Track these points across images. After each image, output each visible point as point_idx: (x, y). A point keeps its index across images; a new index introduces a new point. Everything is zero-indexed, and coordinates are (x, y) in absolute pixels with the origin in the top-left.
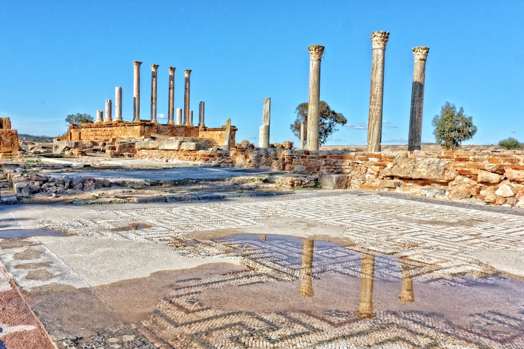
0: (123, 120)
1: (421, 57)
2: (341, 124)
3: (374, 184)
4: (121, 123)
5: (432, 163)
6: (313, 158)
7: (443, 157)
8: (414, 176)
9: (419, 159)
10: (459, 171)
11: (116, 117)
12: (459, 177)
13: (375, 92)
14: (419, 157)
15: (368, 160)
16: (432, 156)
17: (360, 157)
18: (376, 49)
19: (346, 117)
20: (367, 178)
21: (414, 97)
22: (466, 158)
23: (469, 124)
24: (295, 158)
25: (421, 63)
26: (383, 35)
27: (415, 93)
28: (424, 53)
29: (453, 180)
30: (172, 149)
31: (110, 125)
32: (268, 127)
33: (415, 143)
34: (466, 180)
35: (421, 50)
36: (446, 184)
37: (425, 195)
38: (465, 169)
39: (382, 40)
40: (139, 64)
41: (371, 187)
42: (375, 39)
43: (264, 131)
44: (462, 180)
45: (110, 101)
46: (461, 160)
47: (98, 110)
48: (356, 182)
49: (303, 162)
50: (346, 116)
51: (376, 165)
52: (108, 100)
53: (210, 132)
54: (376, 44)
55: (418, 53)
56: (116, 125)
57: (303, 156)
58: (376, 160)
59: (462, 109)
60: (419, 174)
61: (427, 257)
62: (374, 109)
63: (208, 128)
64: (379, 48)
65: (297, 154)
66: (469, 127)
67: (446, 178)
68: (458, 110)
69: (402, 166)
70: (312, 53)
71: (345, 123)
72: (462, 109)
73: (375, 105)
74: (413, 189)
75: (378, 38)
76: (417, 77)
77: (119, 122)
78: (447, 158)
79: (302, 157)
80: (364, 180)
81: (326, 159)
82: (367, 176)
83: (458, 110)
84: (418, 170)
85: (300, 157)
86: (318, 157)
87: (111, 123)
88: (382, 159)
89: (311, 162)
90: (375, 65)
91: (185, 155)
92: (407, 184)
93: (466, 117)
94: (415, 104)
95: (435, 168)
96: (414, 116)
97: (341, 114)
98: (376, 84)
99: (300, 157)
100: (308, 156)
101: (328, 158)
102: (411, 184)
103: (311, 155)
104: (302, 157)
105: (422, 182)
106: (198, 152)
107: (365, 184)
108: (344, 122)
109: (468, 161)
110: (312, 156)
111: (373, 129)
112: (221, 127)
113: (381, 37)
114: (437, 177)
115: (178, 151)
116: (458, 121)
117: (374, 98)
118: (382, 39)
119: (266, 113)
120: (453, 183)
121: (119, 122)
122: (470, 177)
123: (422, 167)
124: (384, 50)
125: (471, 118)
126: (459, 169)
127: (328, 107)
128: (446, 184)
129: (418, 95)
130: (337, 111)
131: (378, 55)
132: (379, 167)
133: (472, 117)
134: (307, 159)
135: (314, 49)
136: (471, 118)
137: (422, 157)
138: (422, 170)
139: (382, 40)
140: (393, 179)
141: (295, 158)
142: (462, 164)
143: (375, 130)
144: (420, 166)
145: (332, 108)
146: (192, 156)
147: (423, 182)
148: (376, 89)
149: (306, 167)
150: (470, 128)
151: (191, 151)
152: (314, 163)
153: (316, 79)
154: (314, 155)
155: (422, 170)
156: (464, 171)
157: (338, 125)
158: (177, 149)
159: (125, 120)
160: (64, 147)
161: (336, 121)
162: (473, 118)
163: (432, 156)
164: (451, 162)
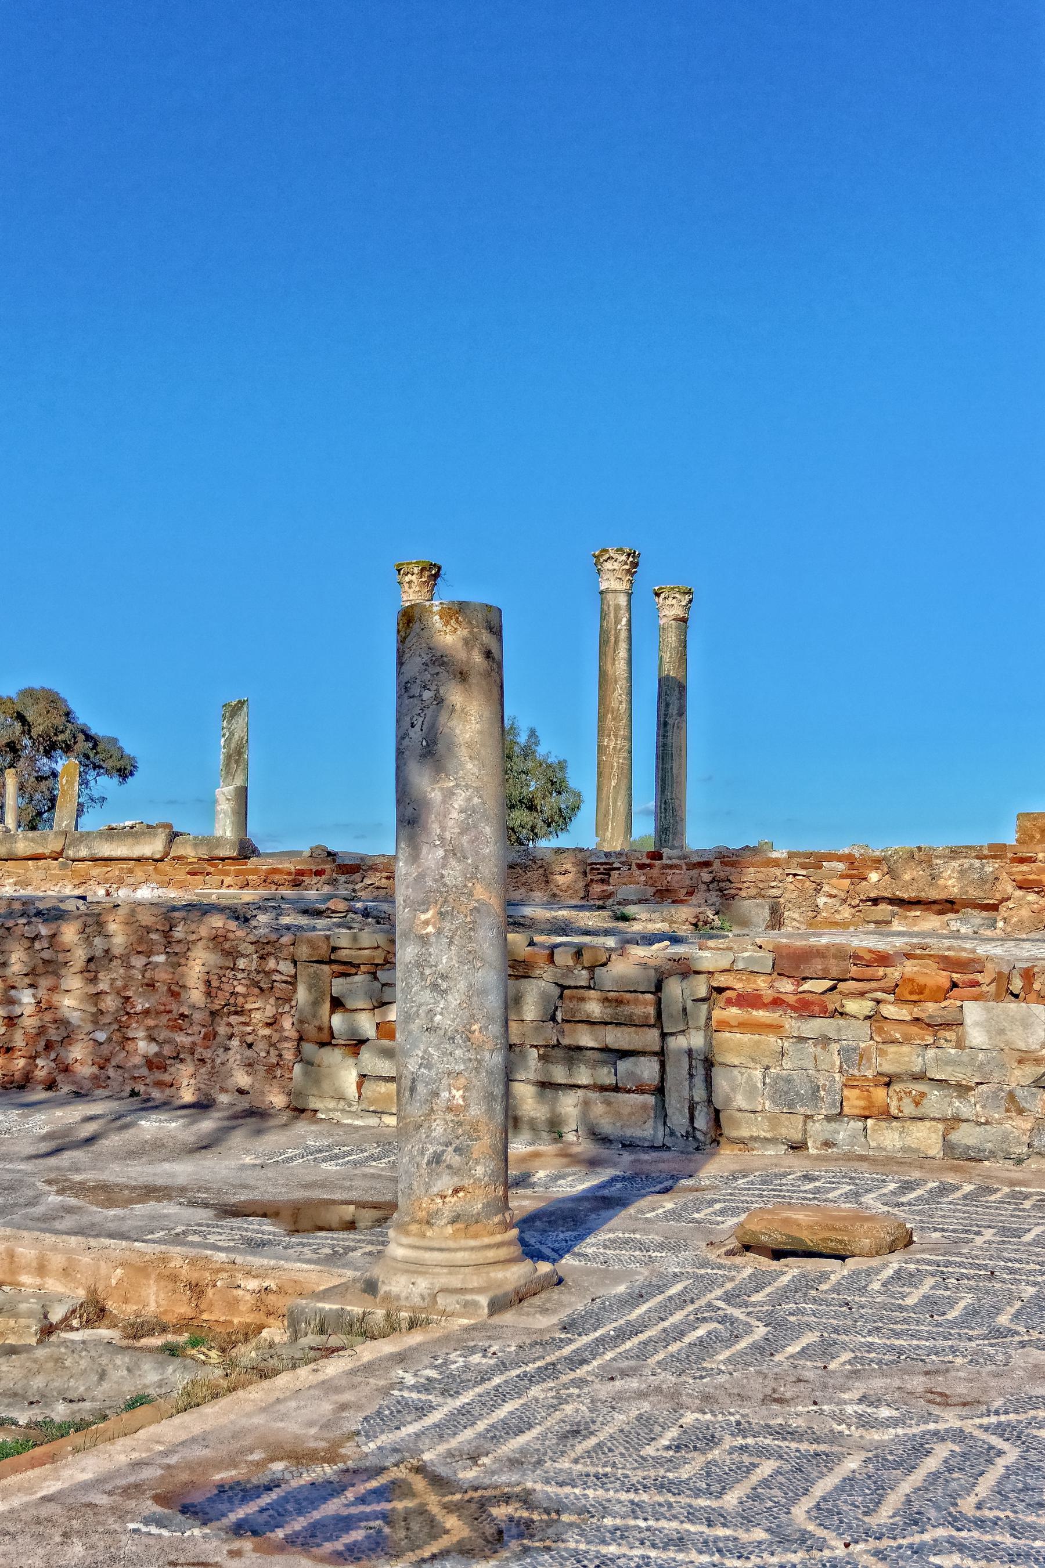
1: (678, 612)
2: (116, 780)
3: (838, 917)
5: (969, 868)
6: (671, 867)
7: (986, 857)
8: (934, 894)
9: (938, 861)
10: (1020, 882)
12: (1019, 893)
13: (614, 704)
14: (937, 857)
15: (821, 867)
16: (964, 854)
17: (803, 860)
18: (612, 592)
19: (128, 750)
20: (821, 905)
21: (666, 715)
22: (1031, 857)
23: (556, 785)
24: (619, 869)
26: (631, 559)
27: (667, 705)
28: (684, 603)
29: (1009, 899)
33: (674, 839)
34: (1031, 897)
35: (677, 595)
36: (994, 908)
37: (958, 931)
38: (1031, 877)
39: (628, 571)
41: (836, 924)
42: (608, 565)
44: (1023, 898)
46: (1022, 861)
48: (796, 916)
49: (643, 878)
50: (130, 747)
51: (843, 877)
54: (612, 579)
55: (670, 601)
57: (644, 864)
59: (533, 733)
60: (943, 890)
61: (157, 1341)
62: (614, 748)
64: (620, 592)
65: (623, 859)
66: (559, 793)
67: (998, 896)
68: (523, 739)
69: (907, 877)
70: (410, 582)
71: (132, 774)
72: (533, 733)
73: (616, 736)
74: (922, 923)
75: (616, 566)
76: (670, 662)
78: (995, 857)
79: (641, 866)
80: (816, 909)
81: (710, 869)
82: (821, 901)
83: (523, 739)
84: (941, 882)
85: (634, 867)
86: (686, 864)
88: (856, 864)
89: (669, 878)
90: (613, 632)
92: (908, 914)
93: (549, 761)
94: (670, 734)
95: (976, 876)
96: (668, 766)
97: (114, 741)
98: (616, 682)
99: (634, 867)
100: (657, 863)
101: (717, 865)
102: (918, 913)
103: (665, 861)
104: (641, 866)
105: (939, 907)
107: (819, 918)
108: (124, 773)
109: (1034, 862)
110: (669, 862)
111: (615, 801)
113: (626, 564)
114: (982, 894)
115: (161, 860)
116: (526, 773)
117: (614, 719)
118: (627, 567)
119: (233, 746)
120: (1010, 904)
122: (1038, 893)
123: (950, 877)
125: (562, 765)
126: (1019, 877)
127: (67, 714)
128: (994, 908)
129: (675, 712)
130: (97, 729)
131: (617, 607)
132: (849, 881)
133: (565, 761)
134: (655, 872)
135: (416, 570)
136: (562, 765)
137: (945, 857)
138: (950, 883)
139: (628, 571)
140: (876, 905)
141: (619, 869)
142: (1024, 868)
143: (619, 804)
144: (945, 875)
145: (84, 717)
147: (948, 906)
148: (616, 694)
149: (653, 890)
150: (564, 796)
152: (677, 878)
155: (950, 883)
156: (1030, 881)
157: (103, 780)
161: (96, 767)
162: (569, 764)
163: (964, 854)
164: (1002, 864)
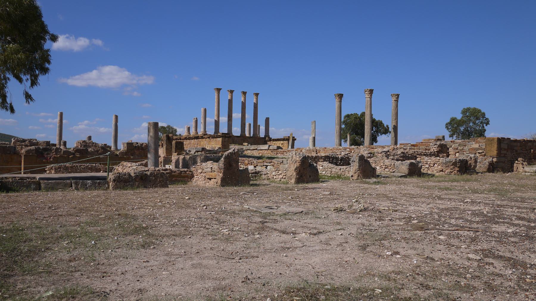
0: (207, 133)
4: (206, 136)
11: (201, 132)
25: (395, 102)
30: (265, 149)
31: (197, 138)
32: (314, 138)
35: (395, 96)
39: (369, 94)
40: (219, 90)
43: (312, 140)
45: (196, 118)
47: (186, 126)
52: (195, 118)
53: (274, 142)
56: (202, 138)
58: (349, 150)
63: (272, 139)
77: (204, 135)
87: (197, 136)
91: (272, 152)
106: (278, 150)
112: (283, 138)
121: (204, 135)
124: (371, 98)
143: (368, 138)
146: (275, 152)
151: (275, 150)
153: (339, 112)
154: (328, 149)
158: (267, 149)
159: (208, 133)
160: (195, 151)
